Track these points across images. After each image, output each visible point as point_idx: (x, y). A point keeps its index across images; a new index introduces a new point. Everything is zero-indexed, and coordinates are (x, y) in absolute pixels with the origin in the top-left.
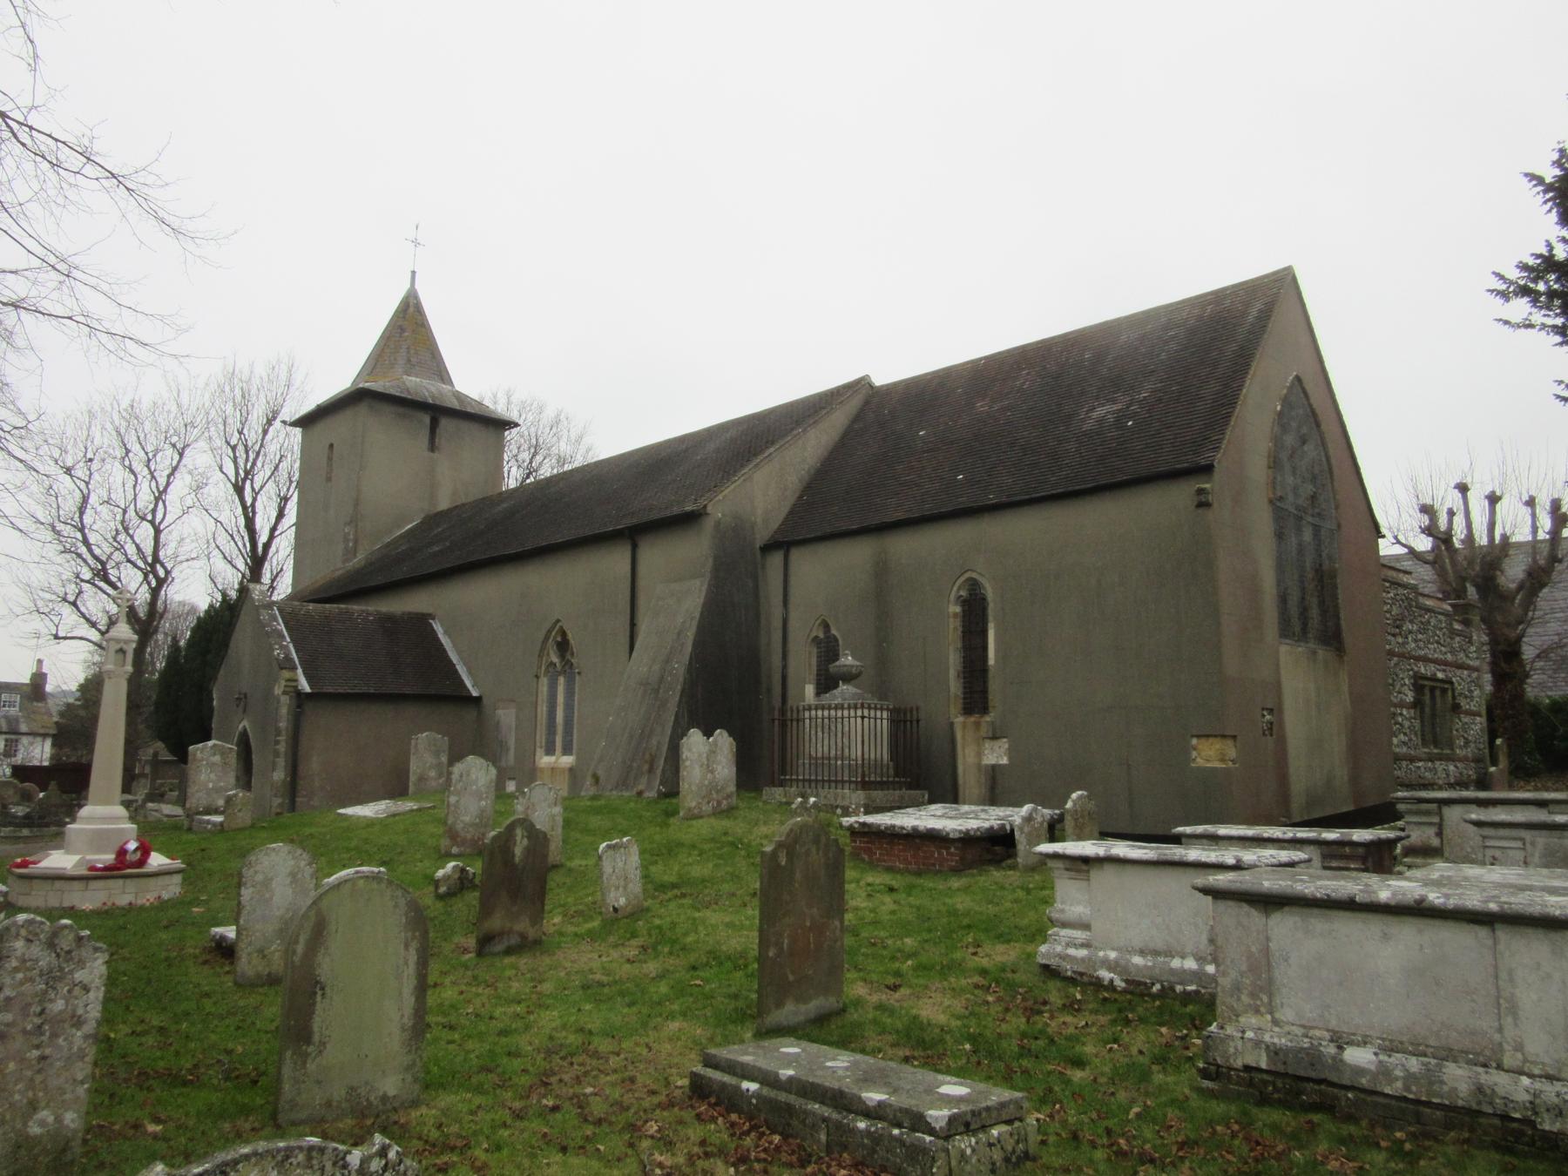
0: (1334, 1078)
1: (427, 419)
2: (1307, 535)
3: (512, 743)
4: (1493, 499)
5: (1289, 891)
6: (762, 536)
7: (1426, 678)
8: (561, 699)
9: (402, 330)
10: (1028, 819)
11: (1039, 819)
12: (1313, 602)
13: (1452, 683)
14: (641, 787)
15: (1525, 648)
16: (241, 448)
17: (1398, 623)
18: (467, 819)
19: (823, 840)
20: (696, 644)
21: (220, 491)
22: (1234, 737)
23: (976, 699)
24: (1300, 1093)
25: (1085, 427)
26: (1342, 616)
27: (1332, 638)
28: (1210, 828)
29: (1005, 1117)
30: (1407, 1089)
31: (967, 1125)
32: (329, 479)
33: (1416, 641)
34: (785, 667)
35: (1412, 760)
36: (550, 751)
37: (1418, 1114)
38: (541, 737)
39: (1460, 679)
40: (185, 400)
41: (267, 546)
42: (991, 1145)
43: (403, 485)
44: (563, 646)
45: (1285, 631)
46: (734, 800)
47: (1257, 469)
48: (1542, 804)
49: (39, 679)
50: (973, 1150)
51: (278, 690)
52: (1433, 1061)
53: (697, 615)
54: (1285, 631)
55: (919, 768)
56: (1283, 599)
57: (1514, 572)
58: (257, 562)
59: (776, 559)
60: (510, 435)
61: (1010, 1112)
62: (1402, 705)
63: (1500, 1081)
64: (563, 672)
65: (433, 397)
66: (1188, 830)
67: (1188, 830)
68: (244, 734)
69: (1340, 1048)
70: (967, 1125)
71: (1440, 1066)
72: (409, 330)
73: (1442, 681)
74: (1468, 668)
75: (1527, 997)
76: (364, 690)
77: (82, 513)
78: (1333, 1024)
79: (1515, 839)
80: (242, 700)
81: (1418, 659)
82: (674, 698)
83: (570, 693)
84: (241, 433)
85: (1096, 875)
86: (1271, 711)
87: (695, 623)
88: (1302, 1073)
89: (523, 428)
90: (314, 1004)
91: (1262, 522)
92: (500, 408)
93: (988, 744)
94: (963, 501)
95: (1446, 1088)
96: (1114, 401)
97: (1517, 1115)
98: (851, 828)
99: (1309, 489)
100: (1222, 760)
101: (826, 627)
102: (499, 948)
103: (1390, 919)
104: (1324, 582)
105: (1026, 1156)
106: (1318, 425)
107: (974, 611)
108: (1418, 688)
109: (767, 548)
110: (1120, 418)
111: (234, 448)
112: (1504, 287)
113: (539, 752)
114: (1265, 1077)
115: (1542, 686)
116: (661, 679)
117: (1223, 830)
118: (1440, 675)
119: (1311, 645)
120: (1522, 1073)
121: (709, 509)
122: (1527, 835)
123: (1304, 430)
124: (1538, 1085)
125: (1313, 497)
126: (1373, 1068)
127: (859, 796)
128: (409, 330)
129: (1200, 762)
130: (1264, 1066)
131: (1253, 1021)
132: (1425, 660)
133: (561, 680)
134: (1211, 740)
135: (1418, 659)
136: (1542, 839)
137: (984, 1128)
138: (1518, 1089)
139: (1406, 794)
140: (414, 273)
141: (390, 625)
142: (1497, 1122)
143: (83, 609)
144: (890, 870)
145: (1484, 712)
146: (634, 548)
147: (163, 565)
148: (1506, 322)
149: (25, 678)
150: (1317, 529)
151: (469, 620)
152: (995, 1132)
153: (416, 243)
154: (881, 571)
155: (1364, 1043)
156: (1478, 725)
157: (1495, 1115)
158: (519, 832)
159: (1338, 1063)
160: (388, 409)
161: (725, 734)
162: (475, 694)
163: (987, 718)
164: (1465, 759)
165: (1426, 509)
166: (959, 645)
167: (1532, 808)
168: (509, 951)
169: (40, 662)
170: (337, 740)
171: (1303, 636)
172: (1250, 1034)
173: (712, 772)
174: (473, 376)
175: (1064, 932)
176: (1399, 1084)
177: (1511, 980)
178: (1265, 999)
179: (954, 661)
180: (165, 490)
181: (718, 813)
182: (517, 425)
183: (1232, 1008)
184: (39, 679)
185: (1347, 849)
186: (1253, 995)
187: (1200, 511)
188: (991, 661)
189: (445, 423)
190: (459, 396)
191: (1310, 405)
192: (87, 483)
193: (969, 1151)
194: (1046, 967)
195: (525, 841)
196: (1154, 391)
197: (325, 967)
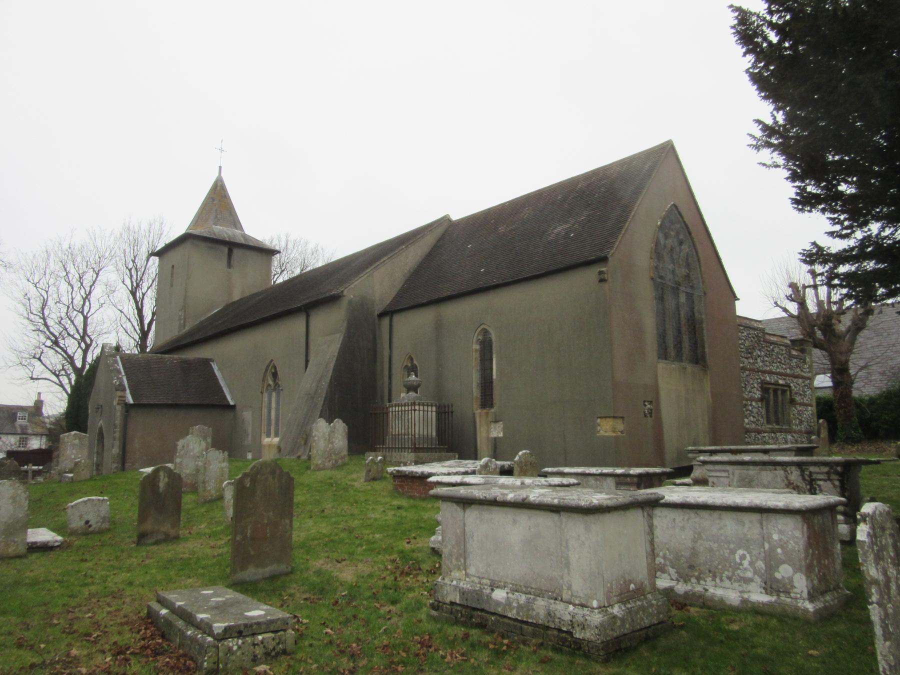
0: (486, 607)
1: (226, 250)
2: (683, 299)
3: (250, 430)
5: (469, 495)
6: (378, 309)
7: (771, 384)
8: (273, 405)
9: (214, 200)
11: (493, 466)
12: (686, 338)
13: (790, 387)
14: (299, 454)
15: (851, 365)
16: (133, 271)
17: (749, 351)
18: (188, 472)
19: (278, 472)
20: (334, 370)
21: (123, 295)
22: (622, 418)
23: (487, 400)
24: (471, 617)
25: (550, 238)
26: (706, 346)
27: (698, 359)
28: (561, 469)
29: (272, 628)
30: (518, 614)
32: (172, 285)
33: (763, 362)
34: (390, 383)
35: (759, 432)
36: (268, 436)
37: (521, 628)
38: (264, 428)
40: (99, 244)
42: (254, 645)
43: (216, 287)
44: (275, 375)
45: (663, 354)
46: (347, 459)
47: (643, 259)
49: (39, 404)
50: (239, 647)
51: (115, 403)
52: (532, 597)
53: (336, 354)
54: (663, 354)
58: (144, 335)
59: (386, 321)
61: (278, 625)
62: (752, 399)
64: (275, 389)
65: (229, 237)
66: (550, 470)
67: (550, 470)
68: (101, 428)
69: (493, 590)
71: (534, 599)
72: (218, 200)
73: (782, 385)
74: (803, 377)
75: (574, 557)
76: (166, 402)
77: (43, 309)
78: (491, 576)
79: (724, 471)
80: (99, 408)
81: (764, 372)
82: (320, 402)
84: (134, 262)
86: (651, 403)
87: (335, 359)
88: (474, 605)
91: (645, 292)
93: (493, 425)
94: (481, 284)
95: (534, 613)
96: (566, 222)
97: (565, 629)
98: (392, 473)
99: (684, 271)
100: (614, 432)
101: (412, 359)
102: (150, 541)
104: (694, 326)
105: (284, 652)
106: (690, 234)
107: (486, 347)
109: (381, 315)
111: (130, 270)
112: (754, 143)
113: (263, 436)
114: (459, 608)
116: (316, 391)
117: (567, 470)
118: (781, 382)
119: (683, 364)
120: (570, 603)
121: (345, 293)
122: (730, 468)
123: (681, 237)
124: (576, 611)
125: (688, 277)
126: (503, 601)
127: (411, 456)
128: (218, 200)
129: (602, 433)
130: (458, 602)
131: (457, 574)
132: (770, 373)
133: (274, 394)
134: (608, 419)
135: (764, 372)
136: (738, 470)
137: (254, 634)
138: (565, 612)
139: (693, 448)
140: (220, 167)
141: (187, 365)
142: (555, 632)
143: (48, 363)
144: (410, 497)
145: (814, 404)
146: (308, 316)
147: (89, 336)
148: (764, 165)
149: (29, 402)
150: (690, 296)
152: (260, 637)
153: (221, 150)
154: (439, 327)
155: (504, 587)
157: (555, 628)
158: (162, 474)
159: (489, 597)
160: (203, 245)
161: (341, 421)
162: (232, 403)
163: (493, 410)
164: (800, 432)
165: (793, 286)
166: (479, 368)
167: (729, 454)
168: (157, 543)
169: (39, 394)
170: (145, 428)
171: (679, 357)
172: (455, 583)
173: (332, 443)
174: (256, 226)
176: (515, 611)
177: (567, 546)
178: (462, 560)
179: (475, 377)
180: (90, 292)
181: (336, 467)
182: (279, 252)
183: (449, 568)
184: (39, 404)
185: (628, 479)
186: (457, 559)
187: (601, 284)
188: (494, 377)
189: (237, 252)
190: (245, 236)
191: (685, 222)
192: (47, 292)
193: (235, 648)
194: (433, 549)
195: (166, 480)
196: (589, 216)
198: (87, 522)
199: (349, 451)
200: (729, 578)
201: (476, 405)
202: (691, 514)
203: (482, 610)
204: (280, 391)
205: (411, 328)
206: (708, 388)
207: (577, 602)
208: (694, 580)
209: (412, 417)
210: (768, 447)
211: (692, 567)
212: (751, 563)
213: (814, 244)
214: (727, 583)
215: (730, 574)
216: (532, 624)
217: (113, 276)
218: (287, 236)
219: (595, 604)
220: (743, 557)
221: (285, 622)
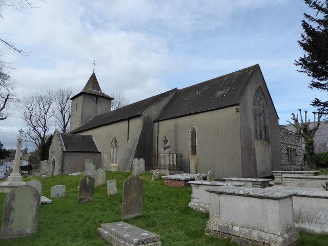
2: (262, 118)
3: (106, 161)
4: (306, 112)
6: (154, 119)
8: (115, 153)
9: (211, 83)
10: (199, 176)
21: (58, 112)
23: (194, 152)
28: (231, 178)
31: (143, 242)
36: (113, 163)
39: (297, 149)
41: (67, 123)
43: (96, 110)
44: (116, 142)
45: (256, 138)
48: (302, 173)
54: (256, 138)
55: (181, 166)
56: (256, 132)
57: (311, 127)
58: (65, 126)
59: (156, 124)
60: (112, 101)
63: (262, 234)
66: (227, 179)
70: (143, 242)
72: (93, 80)
80: (53, 152)
82: (134, 152)
83: (117, 150)
85: (200, 187)
89: (115, 100)
90: (10, 213)
92: (112, 97)
94: (192, 112)
103: (242, 197)
107: (194, 134)
108: (288, 150)
110: (223, 94)
115: (317, 150)
122: (295, 180)
123: (261, 97)
128: (93, 80)
151: (100, 136)
153: (95, 64)
154: (176, 126)
156: (301, 158)
174: (106, 88)
175: (194, 200)
179: (190, 144)
197: (14, 205)
198: (58, 194)
199: (145, 169)
200: (315, 223)
201: (190, 154)
202: (318, 199)
203: (229, 234)
204: (115, 144)
205: (165, 128)
206: (270, 149)
207: (271, 233)
208: (300, 223)
209: (166, 158)
210: (303, 172)
211: (299, 218)
212: (324, 217)
213: (316, 99)
214: (314, 224)
215: (316, 221)
216: (251, 240)
217: (55, 106)
218: (114, 93)
219: (279, 234)
220: (321, 215)
221: (157, 238)
